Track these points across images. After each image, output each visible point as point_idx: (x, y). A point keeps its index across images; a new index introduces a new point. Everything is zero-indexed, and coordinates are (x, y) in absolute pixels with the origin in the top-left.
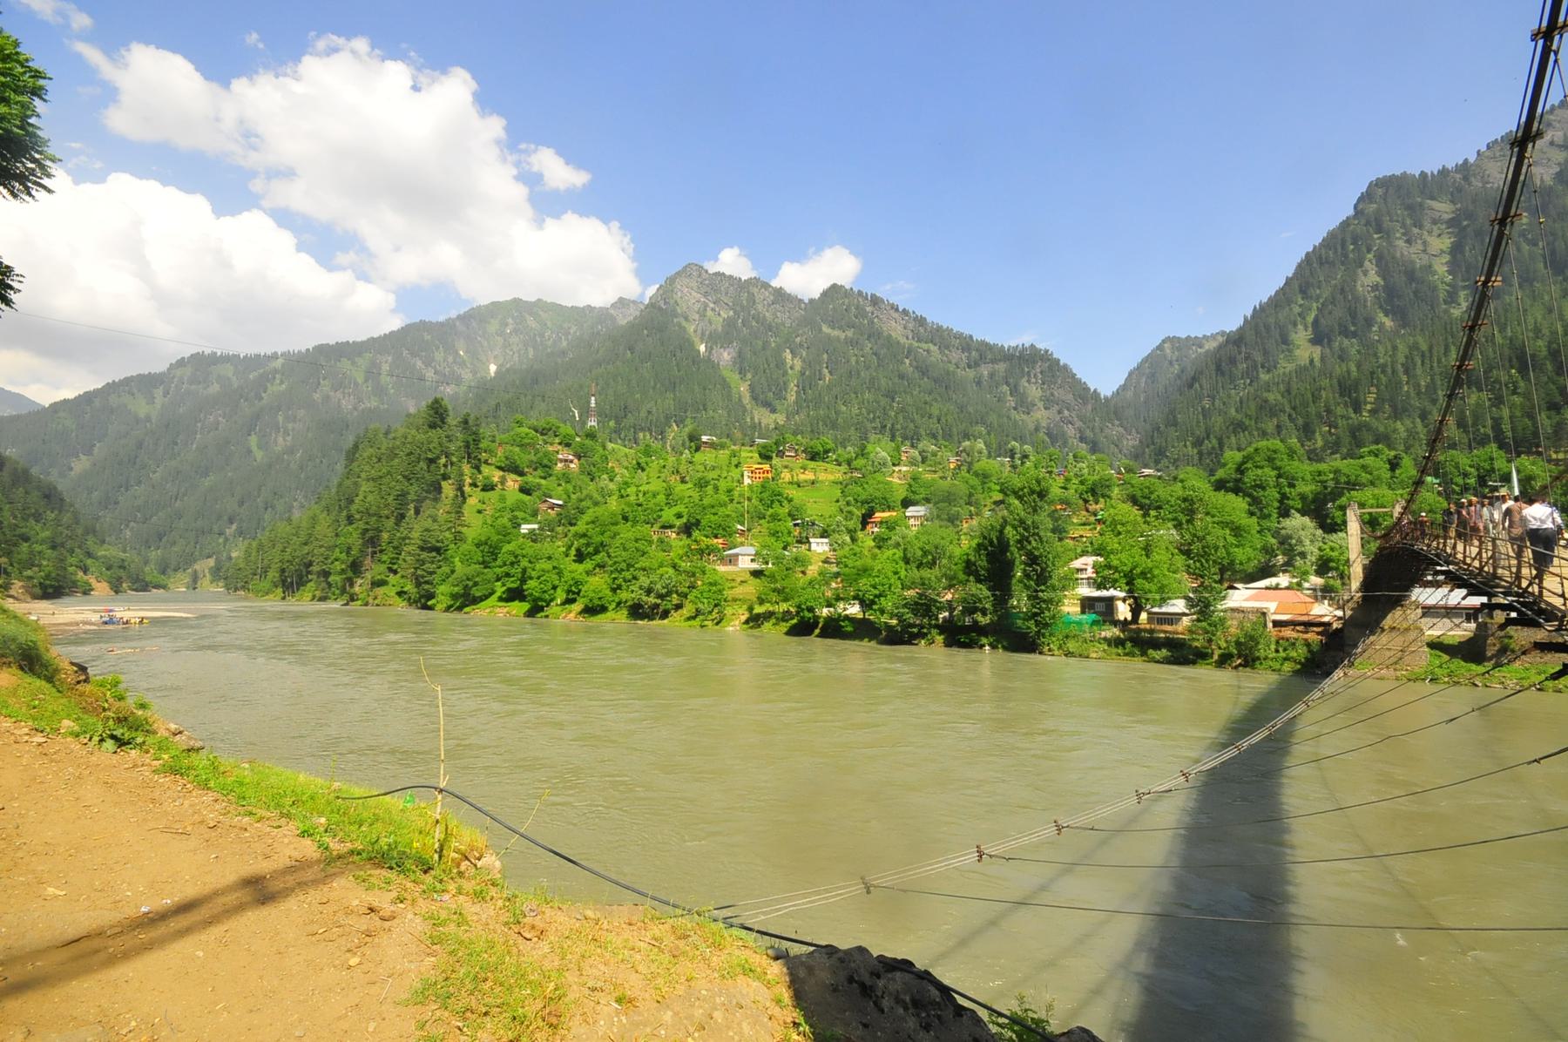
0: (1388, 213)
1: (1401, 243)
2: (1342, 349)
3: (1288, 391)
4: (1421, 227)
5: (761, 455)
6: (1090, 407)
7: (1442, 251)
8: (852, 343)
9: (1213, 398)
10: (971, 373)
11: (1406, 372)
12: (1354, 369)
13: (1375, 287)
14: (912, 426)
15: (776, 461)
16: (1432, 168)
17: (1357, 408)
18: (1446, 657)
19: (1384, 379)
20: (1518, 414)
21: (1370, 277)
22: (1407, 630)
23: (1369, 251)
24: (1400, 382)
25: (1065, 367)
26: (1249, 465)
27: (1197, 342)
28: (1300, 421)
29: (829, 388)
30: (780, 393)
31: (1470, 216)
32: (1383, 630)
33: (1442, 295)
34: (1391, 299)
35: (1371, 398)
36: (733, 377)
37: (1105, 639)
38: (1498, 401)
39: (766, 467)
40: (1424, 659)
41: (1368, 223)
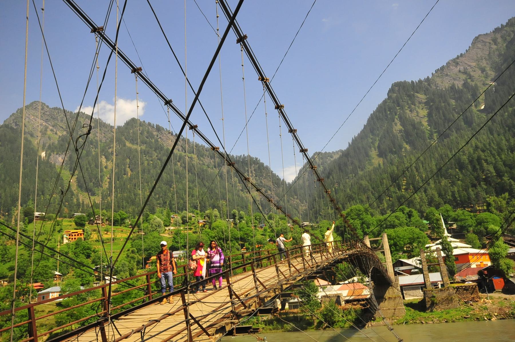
0: (401, 98)
1: (408, 112)
2: (391, 160)
3: (370, 180)
4: (415, 105)
5: (77, 224)
6: (281, 189)
7: (425, 116)
8: (143, 152)
9: (339, 184)
10: (216, 171)
11: (417, 170)
12: (396, 169)
13: (400, 131)
14: (182, 201)
15: (88, 227)
16: (416, 80)
17: (399, 189)
18: (412, 310)
19: (408, 174)
20: (461, 189)
21: (398, 127)
22: (395, 298)
23: (396, 114)
24: (415, 175)
25: (267, 168)
26: (349, 218)
27: (330, 155)
28: (377, 195)
29: (131, 179)
30: (98, 184)
31: (433, 101)
32: (386, 300)
33: (427, 136)
34: (407, 136)
35: (404, 183)
36: (66, 174)
37: (264, 321)
38: (453, 184)
39: (80, 231)
40: (404, 312)
41: (394, 102)
